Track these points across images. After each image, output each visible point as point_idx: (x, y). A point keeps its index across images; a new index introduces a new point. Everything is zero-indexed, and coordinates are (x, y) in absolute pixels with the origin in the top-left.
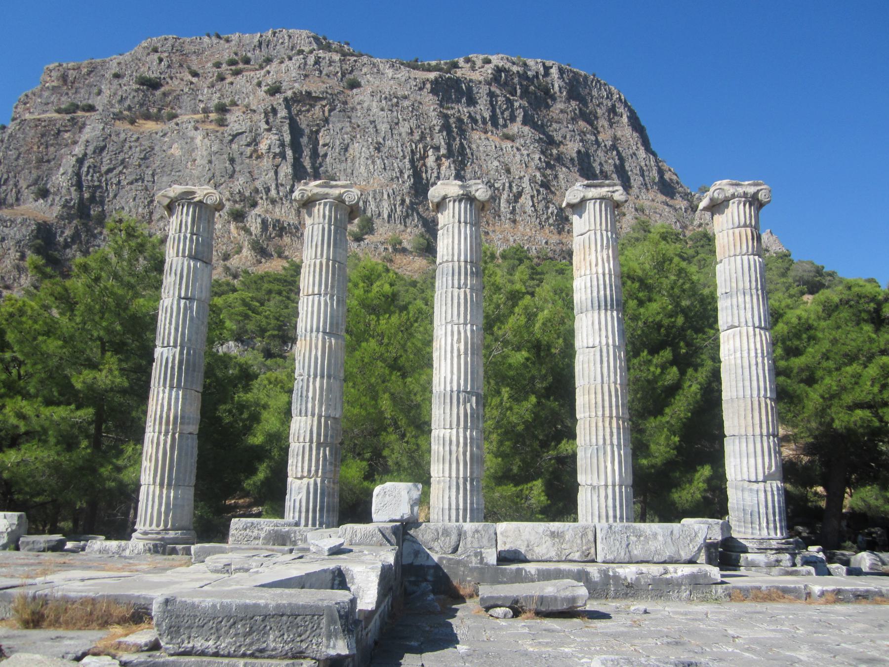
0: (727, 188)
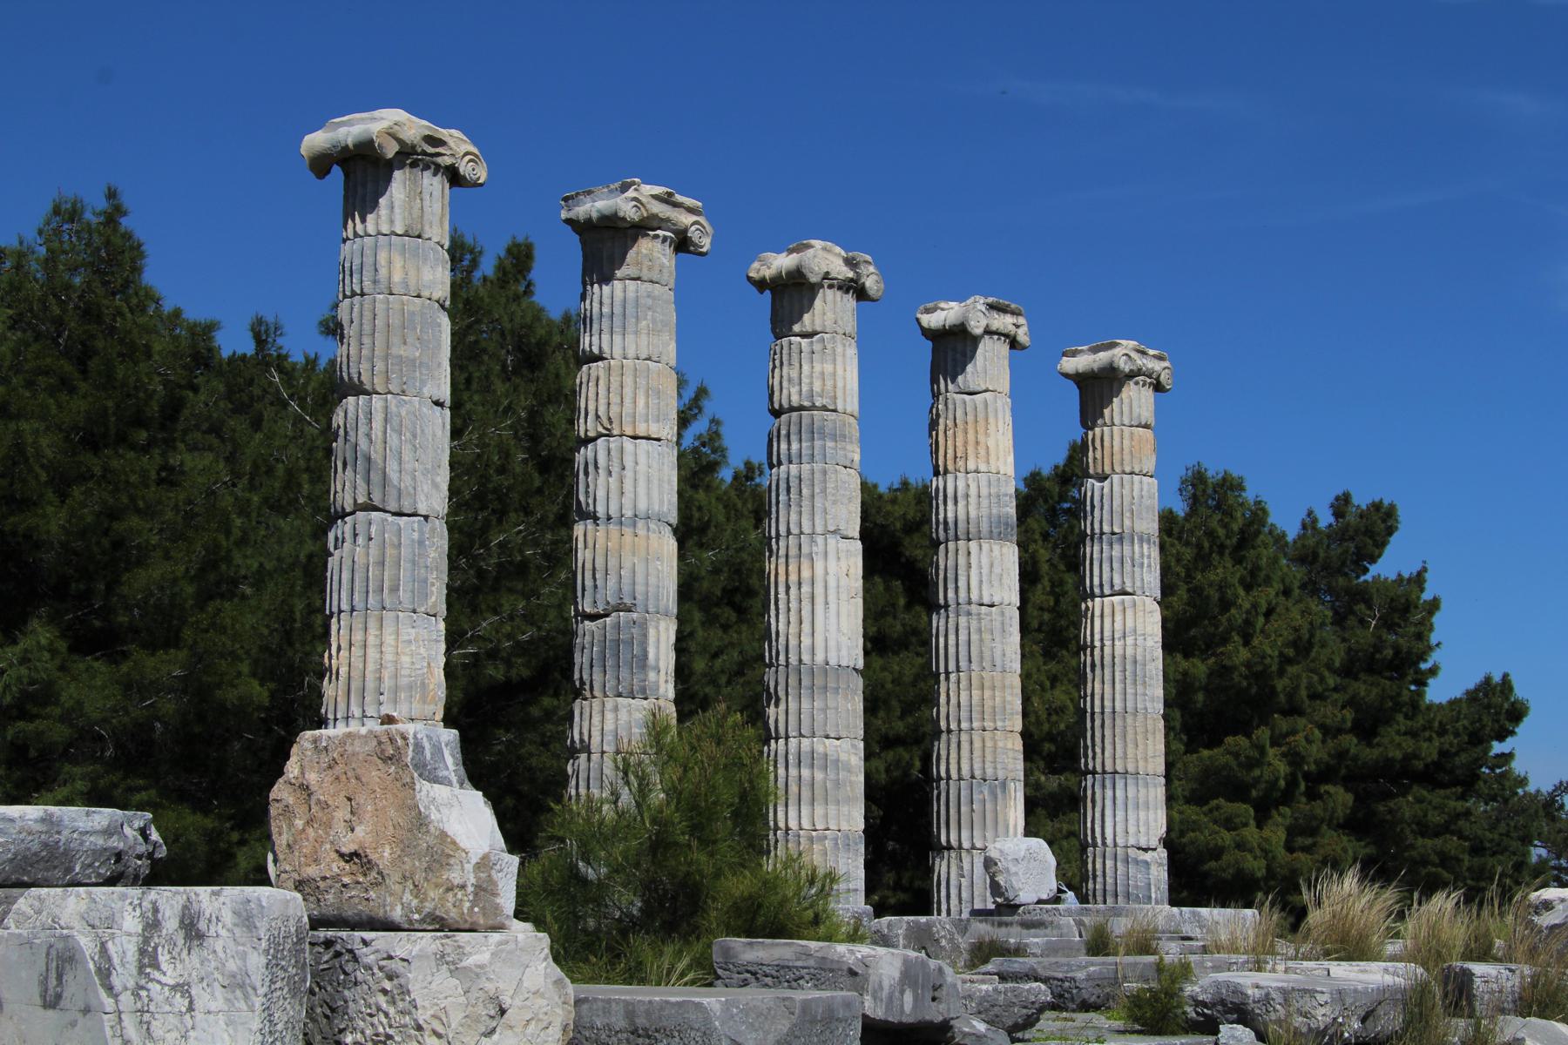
0: (1134, 355)
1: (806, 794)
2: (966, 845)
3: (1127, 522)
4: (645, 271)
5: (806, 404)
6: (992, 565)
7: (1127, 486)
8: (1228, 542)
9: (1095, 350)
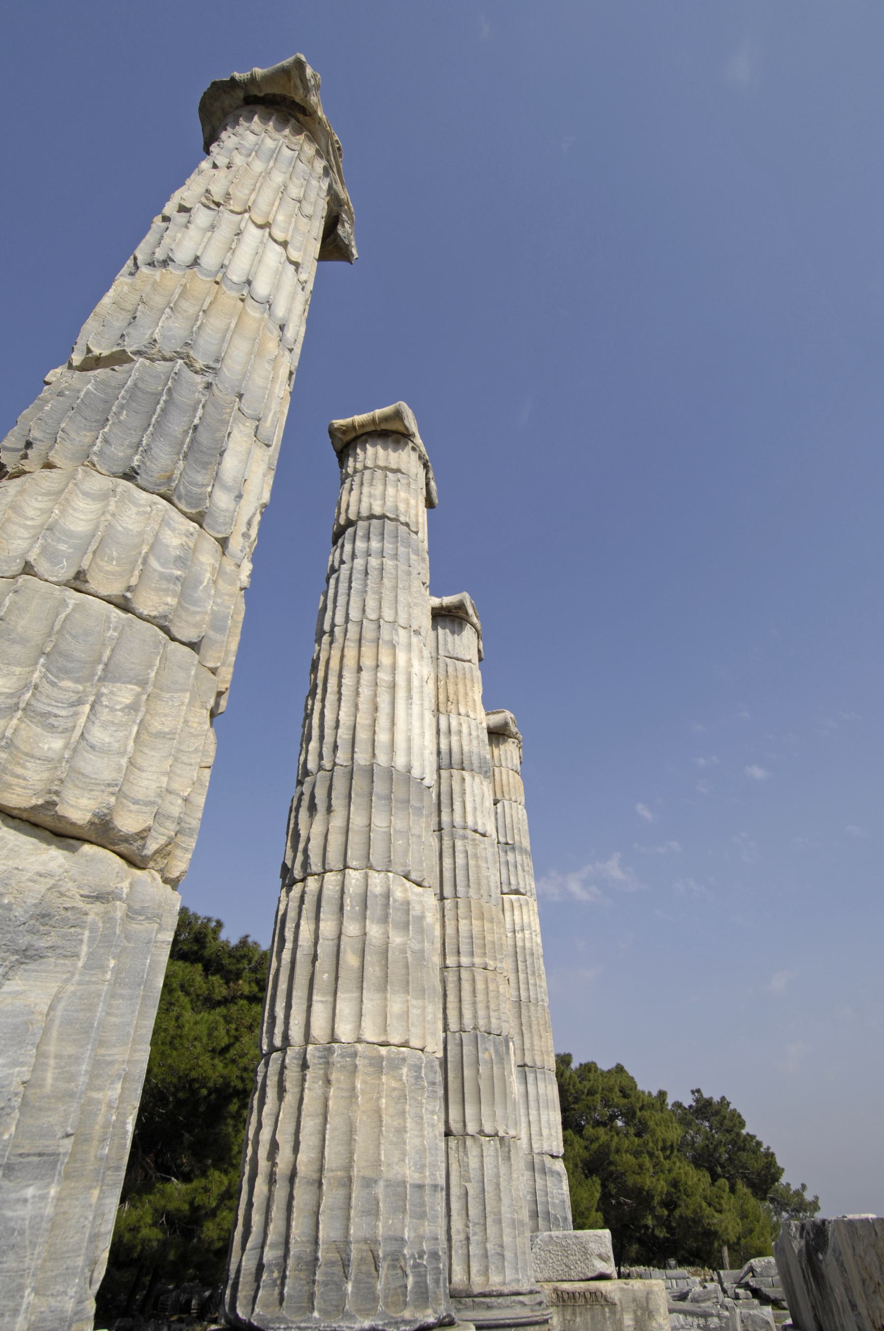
1: (372, 971)
2: (471, 1128)
3: (517, 838)
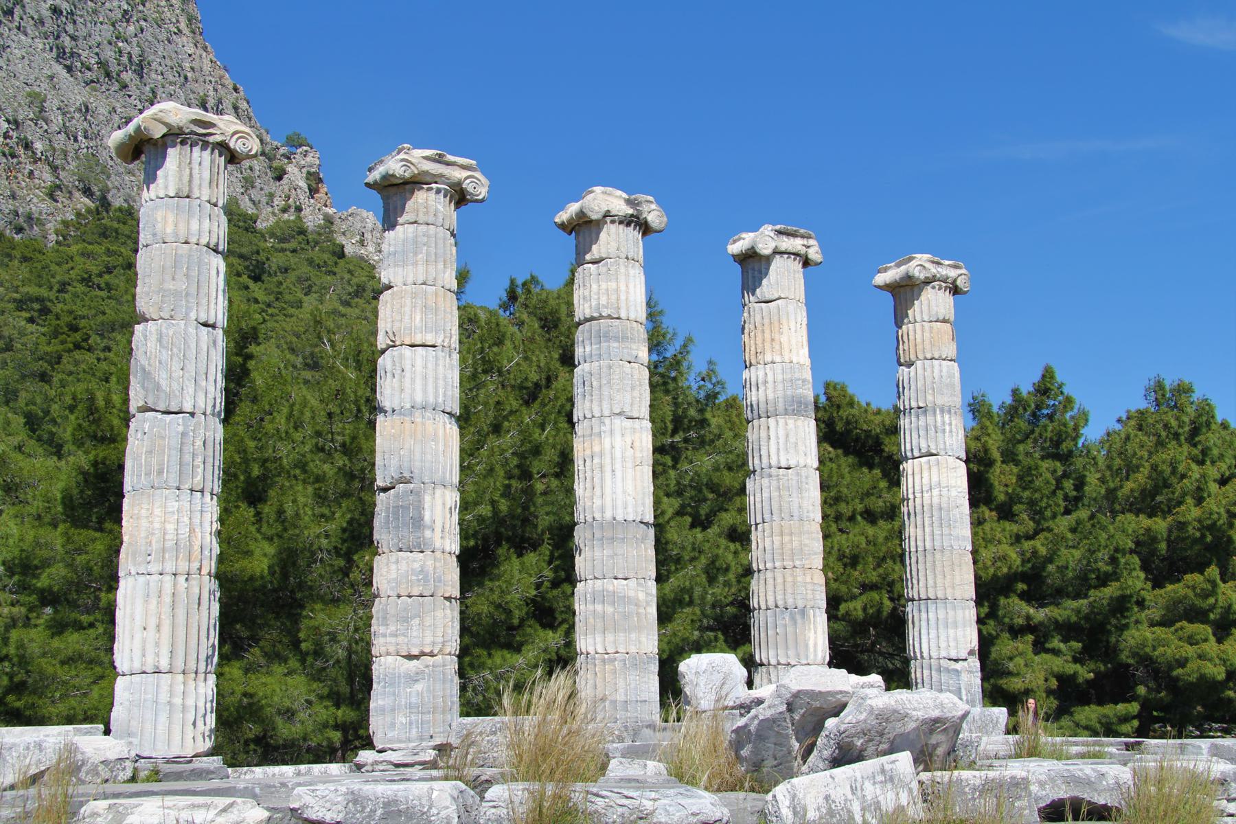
0: (927, 265)
3: (930, 398)
4: (421, 215)
5: (596, 315)
6: (787, 436)
7: (929, 370)
8: (1180, 431)
9: (898, 265)
